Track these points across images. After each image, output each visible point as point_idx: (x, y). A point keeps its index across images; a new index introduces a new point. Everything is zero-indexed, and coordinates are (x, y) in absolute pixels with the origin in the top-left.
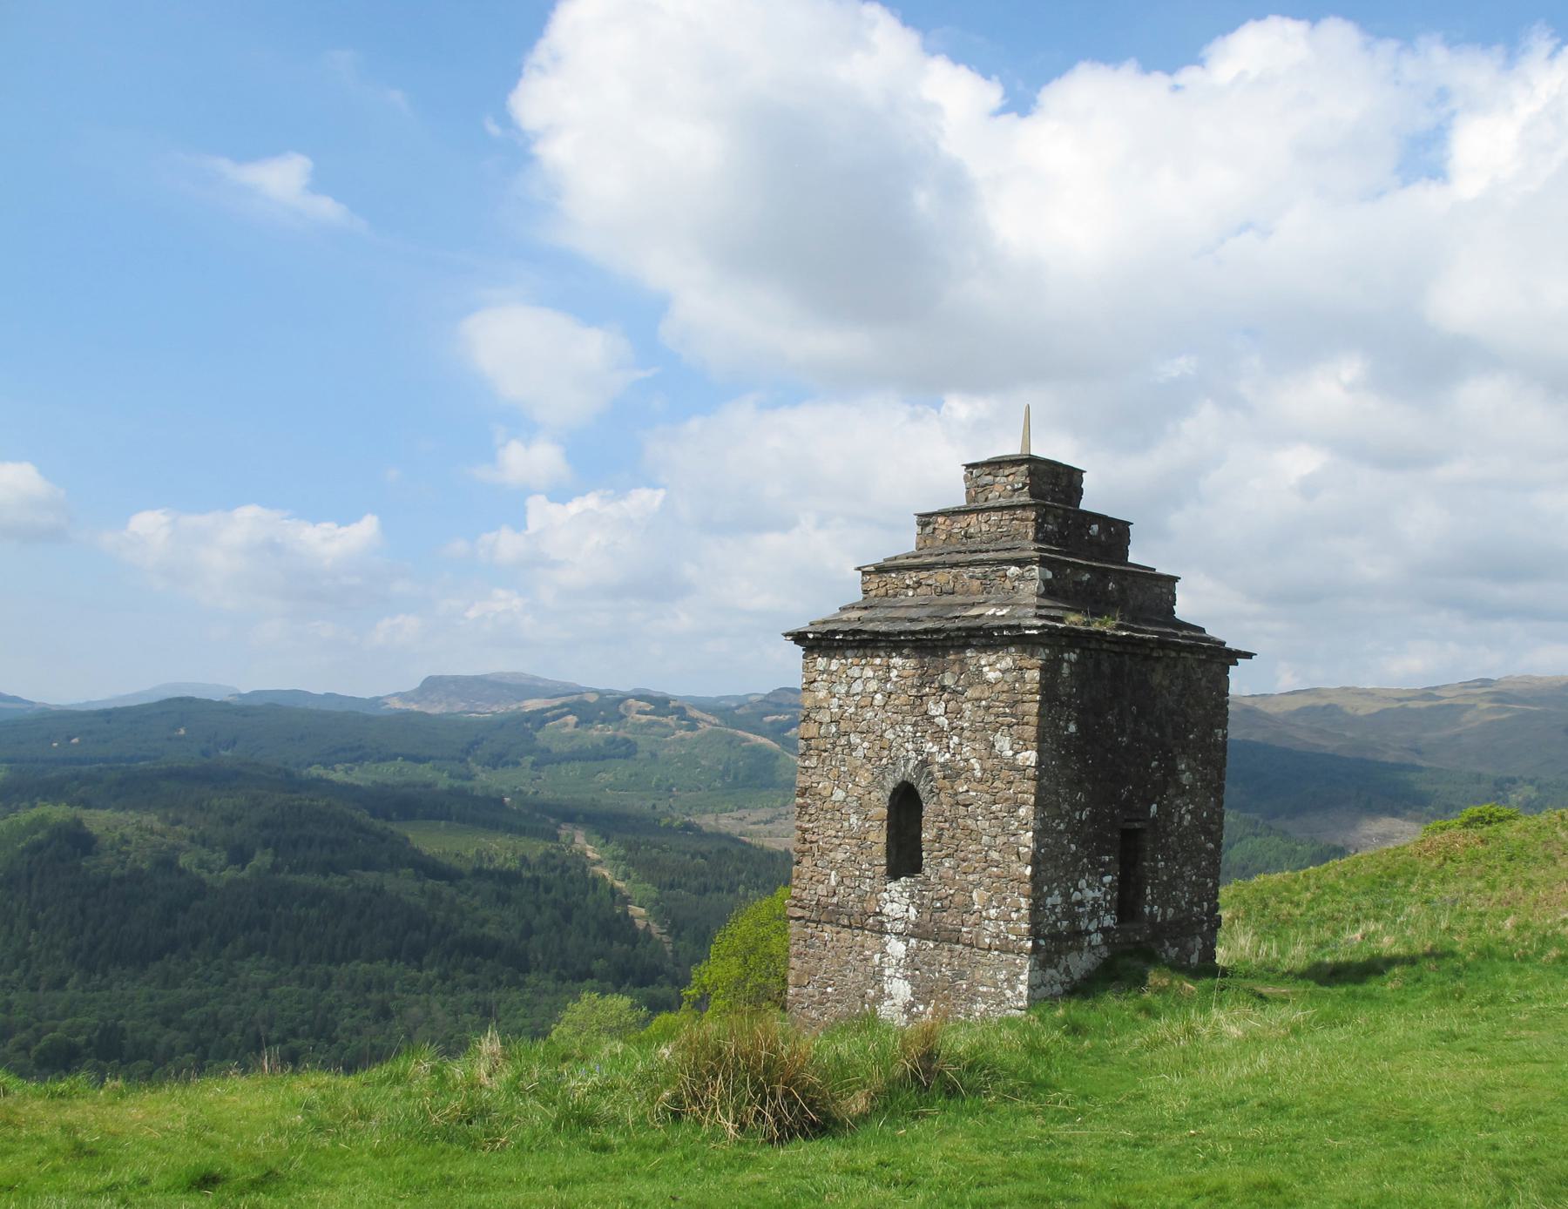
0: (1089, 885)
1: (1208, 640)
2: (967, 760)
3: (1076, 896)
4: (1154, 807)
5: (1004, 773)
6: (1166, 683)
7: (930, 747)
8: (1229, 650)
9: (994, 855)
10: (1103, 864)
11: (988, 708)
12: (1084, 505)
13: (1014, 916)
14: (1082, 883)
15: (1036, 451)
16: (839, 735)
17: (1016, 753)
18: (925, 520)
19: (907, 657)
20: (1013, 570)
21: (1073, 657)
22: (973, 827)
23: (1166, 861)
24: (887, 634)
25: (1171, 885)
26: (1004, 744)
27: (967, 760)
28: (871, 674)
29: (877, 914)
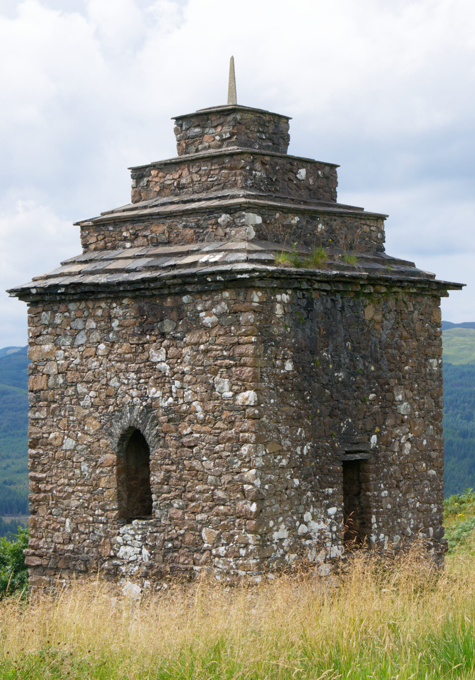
0: (314, 518)
1: (418, 273)
2: (189, 403)
3: (303, 529)
4: (374, 439)
5: (226, 414)
6: (378, 317)
7: (154, 392)
8: (438, 283)
9: (220, 494)
10: (327, 497)
11: (206, 352)
12: (292, 151)
13: (243, 552)
14: (307, 516)
15: (242, 101)
16: (66, 385)
17: (236, 393)
18: (139, 173)
19: (127, 307)
20: (224, 218)
21: (285, 297)
22: (198, 467)
23: (389, 489)
24: (107, 285)
25: (395, 513)
26: (224, 387)
27: (189, 403)
28: (93, 325)
29: (111, 558)
